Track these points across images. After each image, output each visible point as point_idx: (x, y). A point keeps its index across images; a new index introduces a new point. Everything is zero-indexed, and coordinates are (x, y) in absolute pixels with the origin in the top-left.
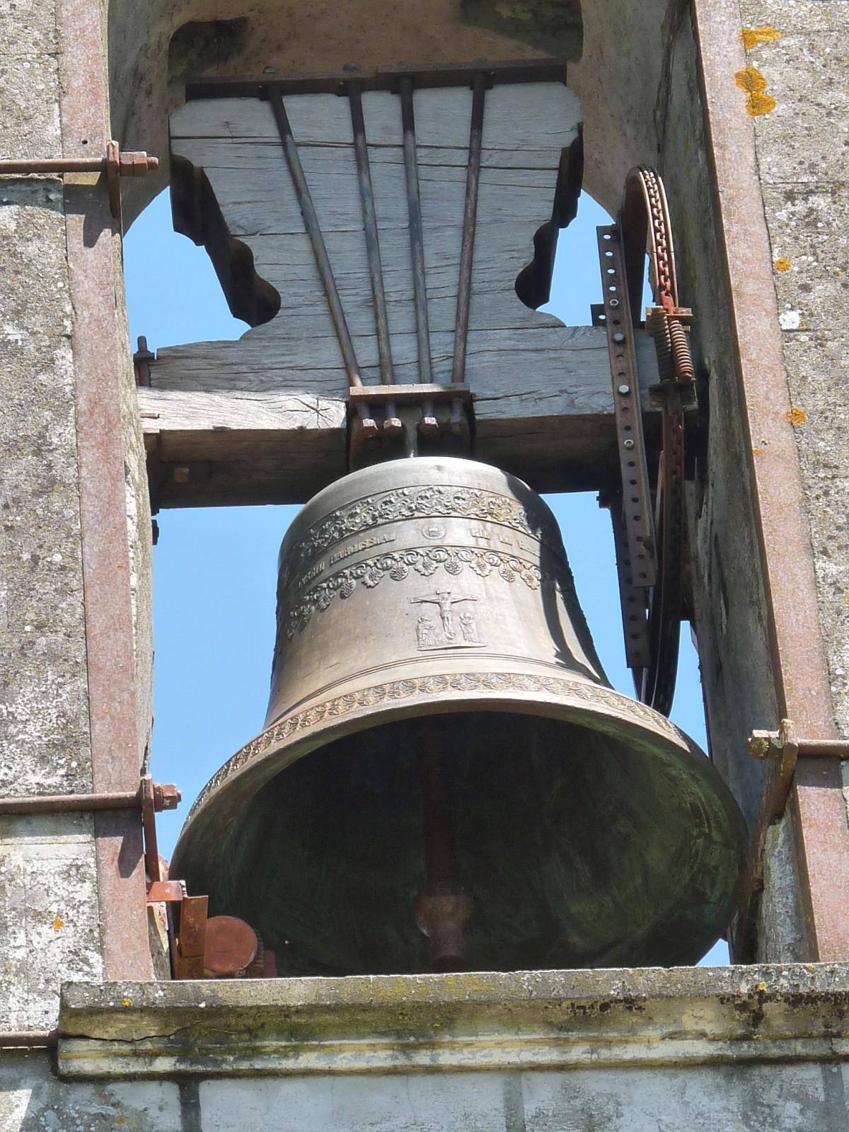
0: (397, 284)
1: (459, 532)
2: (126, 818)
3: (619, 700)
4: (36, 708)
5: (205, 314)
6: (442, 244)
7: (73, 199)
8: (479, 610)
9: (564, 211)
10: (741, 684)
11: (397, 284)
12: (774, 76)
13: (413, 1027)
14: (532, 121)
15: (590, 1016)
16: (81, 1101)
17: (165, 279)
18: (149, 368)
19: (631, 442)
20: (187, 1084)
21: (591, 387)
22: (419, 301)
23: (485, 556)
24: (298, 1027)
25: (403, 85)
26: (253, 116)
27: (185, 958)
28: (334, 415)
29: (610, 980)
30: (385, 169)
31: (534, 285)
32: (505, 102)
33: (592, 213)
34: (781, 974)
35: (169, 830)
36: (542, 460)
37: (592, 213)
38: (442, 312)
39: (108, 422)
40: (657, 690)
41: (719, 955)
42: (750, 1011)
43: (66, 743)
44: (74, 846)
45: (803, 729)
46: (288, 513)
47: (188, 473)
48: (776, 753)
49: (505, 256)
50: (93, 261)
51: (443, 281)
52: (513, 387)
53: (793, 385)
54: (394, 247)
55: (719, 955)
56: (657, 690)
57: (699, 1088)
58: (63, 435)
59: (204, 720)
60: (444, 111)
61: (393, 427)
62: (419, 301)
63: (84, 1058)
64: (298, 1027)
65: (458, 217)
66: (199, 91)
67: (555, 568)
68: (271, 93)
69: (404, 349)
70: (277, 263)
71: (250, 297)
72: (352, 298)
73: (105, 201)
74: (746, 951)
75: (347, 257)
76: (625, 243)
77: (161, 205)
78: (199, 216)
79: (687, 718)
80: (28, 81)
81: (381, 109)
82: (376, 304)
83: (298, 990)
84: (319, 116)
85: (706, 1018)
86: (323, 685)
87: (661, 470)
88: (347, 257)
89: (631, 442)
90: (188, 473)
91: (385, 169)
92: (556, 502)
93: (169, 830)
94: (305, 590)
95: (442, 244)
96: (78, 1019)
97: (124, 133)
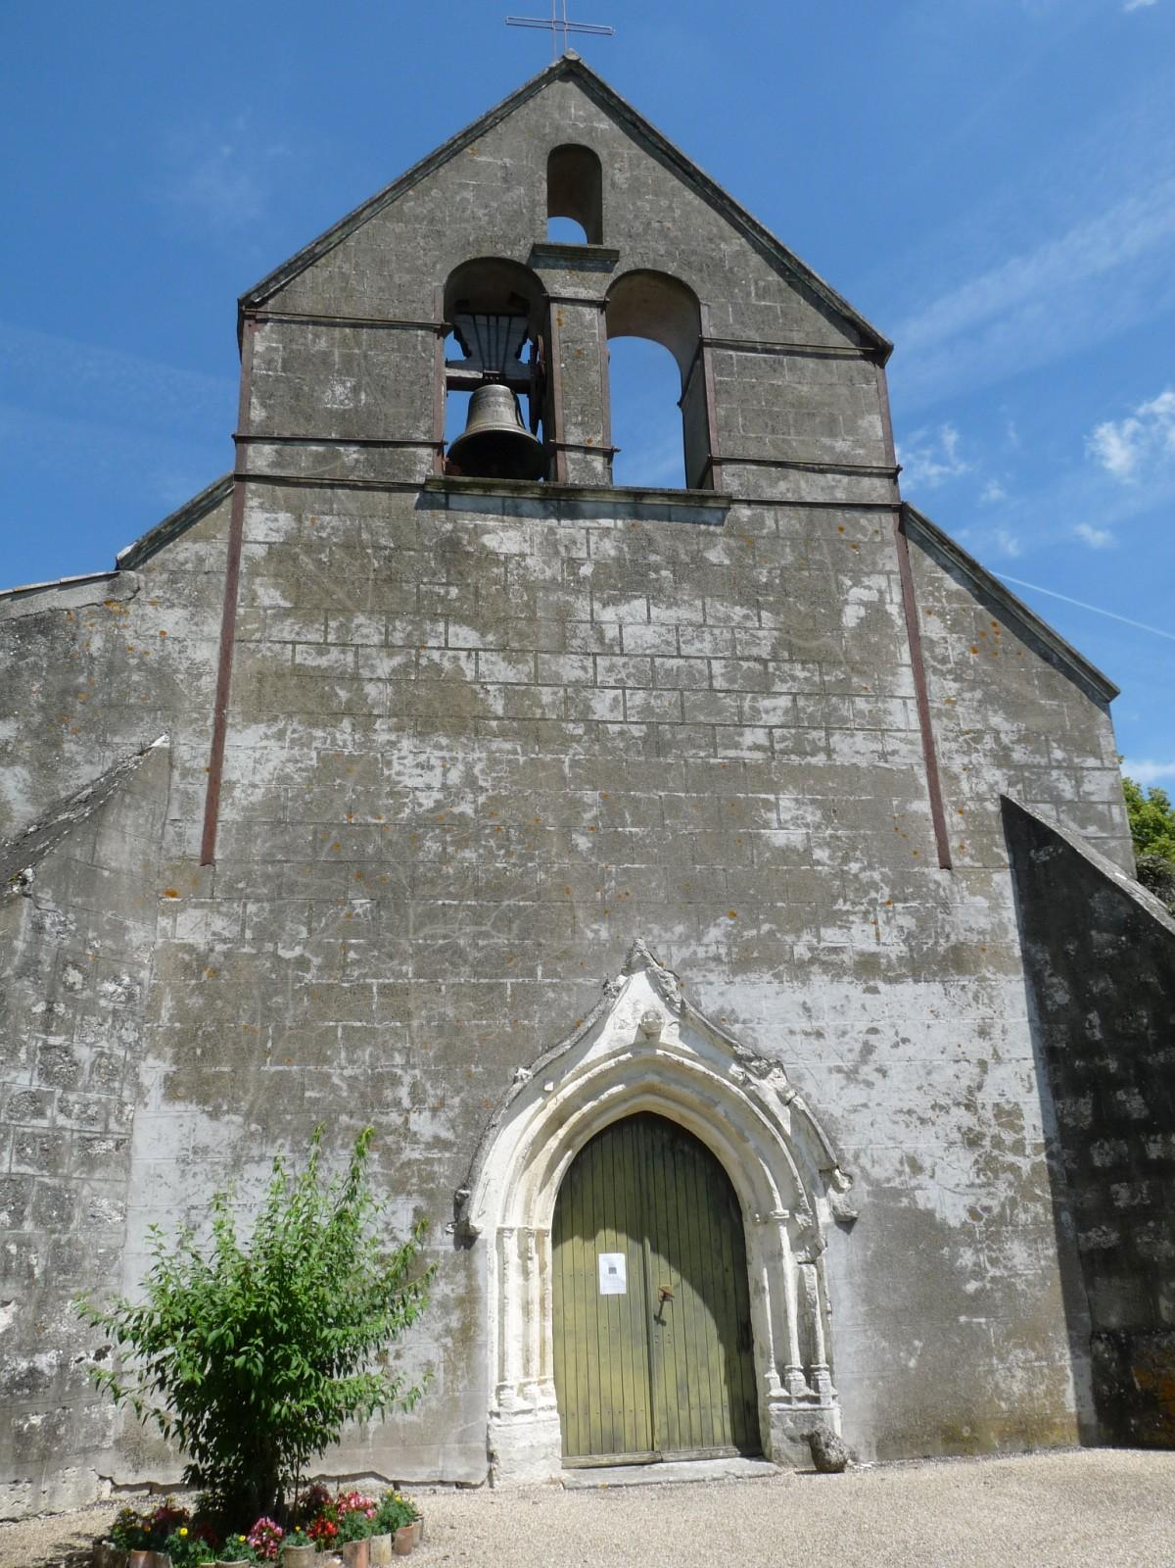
0: (493, 352)
1: (501, 399)
2: (438, 446)
3: (527, 433)
4: (424, 425)
5: (460, 356)
6: (502, 347)
7: (435, 331)
8: (504, 414)
9: (524, 342)
10: (550, 431)
11: (493, 352)
12: (564, 320)
13: (488, 488)
14: (519, 324)
15: (518, 489)
16: (428, 496)
17: (452, 348)
18: (448, 364)
19: (533, 386)
20: (447, 495)
21: (527, 376)
22: (497, 356)
23: (505, 404)
24: (467, 486)
25: (497, 315)
26: (469, 318)
27: (448, 472)
28: (481, 376)
29: (522, 482)
30: (493, 331)
31: (518, 355)
32: (515, 320)
33: (529, 343)
34: (552, 484)
35: (446, 449)
36: (516, 388)
37: (529, 343)
38: (501, 359)
39: (439, 373)
40: (534, 431)
41: (542, 480)
42: (545, 490)
43: (428, 432)
44: (429, 450)
45: (559, 441)
46: (471, 393)
47: (454, 384)
48: (554, 444)
49: (513, 349)
50: (439, 342)
51: (502, 352)
52: (512, 373)
53: (562, 378)
54: (493, 344)
55: (542, 480)
56: (534, 431)
57: (536, 503)
58: (431, 375)
59: (454, 427)
60: (504, 321)
61: (1106, 1068)
62: (497, 356)
63: (429, 489)
64: (467, 486)
65: (384, 495)
66: (461, 313)
67: (518, 408)
68: (473, 315)
69: (494, 364)
70: (472, 347)
71: (466, 352)
72: (485, 354)
73: (442, 332)
74: (546, 479)
75: (485, 346)
76: (534, 349)
77: (452, 334)
78: (458, 337)
79: (539, 437)
80: (429, 307)
81: (493, 319)
82: (489, 356)
83: (467, 479)
84: (482, 320)
85: (538, 491)
86: (346, 1473)
87: (537, 389)
88: (485, 346)
89: (533, 386)
90: (454, 384)
91: (493, 331)
92: (520, 396)
93: (446, 449)
94: (474, 408)
95: (502, 347)
96: (429, 481)
97: (446, 320)
